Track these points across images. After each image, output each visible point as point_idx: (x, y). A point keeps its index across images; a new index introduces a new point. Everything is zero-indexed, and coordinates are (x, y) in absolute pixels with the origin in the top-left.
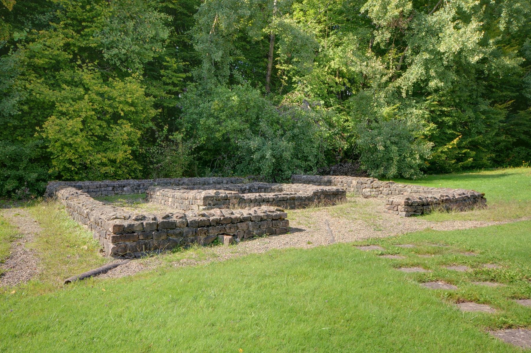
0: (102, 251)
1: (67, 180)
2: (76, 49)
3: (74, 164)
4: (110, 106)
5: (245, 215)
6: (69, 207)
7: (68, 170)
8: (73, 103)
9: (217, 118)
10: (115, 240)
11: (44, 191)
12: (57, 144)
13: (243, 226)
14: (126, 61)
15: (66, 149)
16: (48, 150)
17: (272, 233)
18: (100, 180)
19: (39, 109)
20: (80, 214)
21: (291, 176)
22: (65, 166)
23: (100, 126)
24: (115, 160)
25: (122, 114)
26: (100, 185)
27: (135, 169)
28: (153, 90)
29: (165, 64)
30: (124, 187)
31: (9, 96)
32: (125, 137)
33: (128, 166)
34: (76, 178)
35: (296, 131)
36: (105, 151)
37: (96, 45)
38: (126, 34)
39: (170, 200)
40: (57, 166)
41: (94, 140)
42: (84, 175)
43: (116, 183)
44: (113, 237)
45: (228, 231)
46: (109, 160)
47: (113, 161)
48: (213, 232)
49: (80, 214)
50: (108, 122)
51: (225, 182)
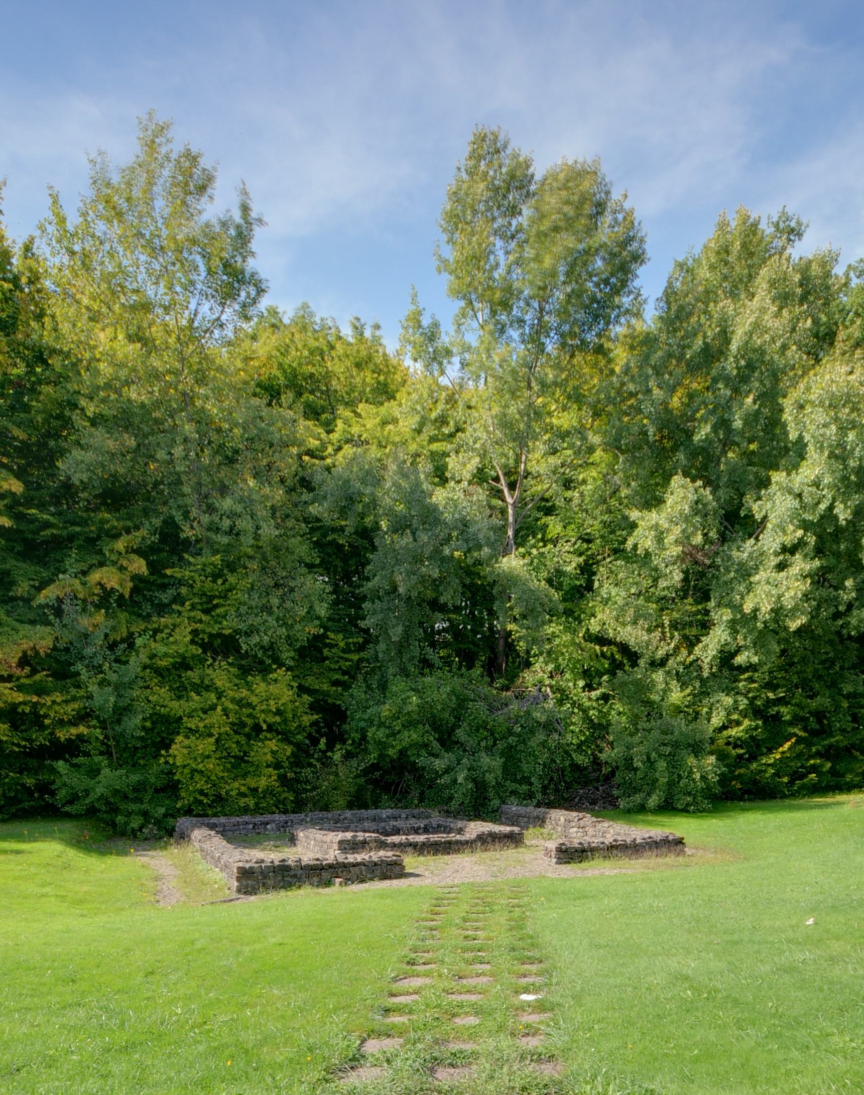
0: (229, 889)
1: (198, 816)
2: (205, 637)
3: (206, 795)
4: (250, 716)
5: (359, 860)
6: (202, 850)
7: (201, 802)
8: (204, 716)
9: (389, 727)
10: (238, 879)
11: (173, 830)
12: (186, 771)
13: (357, 869)
14: (271, 649)
15: (197, 777)
16: (176, 778)
17: (385, 877)
18: (238, 816)
19: (163, 724)
20: (212, 858)
21: (498, 808)
22: (195, 798)
23: (238, 742)
24: (258, 788)
25: (265, 727)
26: (238, 822)
27: (285, 799)
28: (311, 682)
29: (328, 641)
30: (267, 824)
31: (130, 711)
32: (269, 757)
33: (274, 795)
34: (210, 812)
35: (512, 740)
36: (245, 775)
37: (230, 631)
38: (270, 613)
39: (312, 843)
40: (186, 798)
41: (231, 763)
42: (219, 809)
43: (258, 819)
44: (237, 877)
45: (340, 874)
46: (249, 788)
47: (255, 790)
48: (325, 875)
49: (212, 858)
50: (248, 737)
51: (404, 816)
